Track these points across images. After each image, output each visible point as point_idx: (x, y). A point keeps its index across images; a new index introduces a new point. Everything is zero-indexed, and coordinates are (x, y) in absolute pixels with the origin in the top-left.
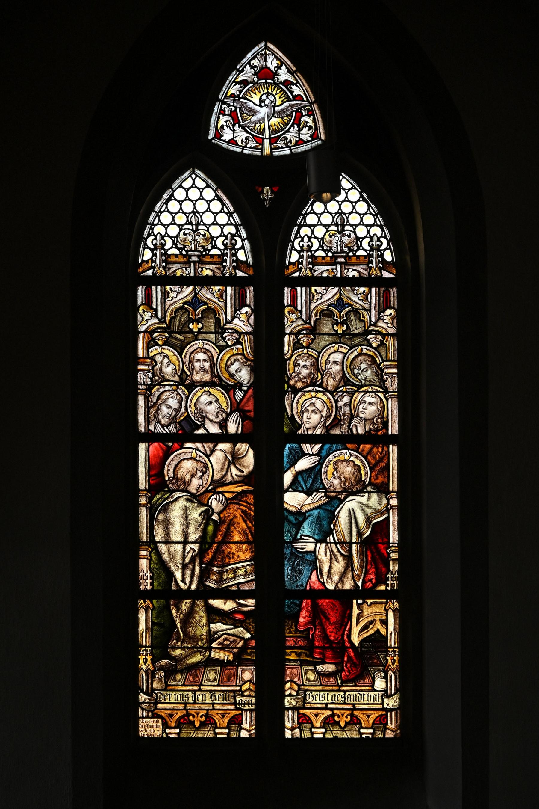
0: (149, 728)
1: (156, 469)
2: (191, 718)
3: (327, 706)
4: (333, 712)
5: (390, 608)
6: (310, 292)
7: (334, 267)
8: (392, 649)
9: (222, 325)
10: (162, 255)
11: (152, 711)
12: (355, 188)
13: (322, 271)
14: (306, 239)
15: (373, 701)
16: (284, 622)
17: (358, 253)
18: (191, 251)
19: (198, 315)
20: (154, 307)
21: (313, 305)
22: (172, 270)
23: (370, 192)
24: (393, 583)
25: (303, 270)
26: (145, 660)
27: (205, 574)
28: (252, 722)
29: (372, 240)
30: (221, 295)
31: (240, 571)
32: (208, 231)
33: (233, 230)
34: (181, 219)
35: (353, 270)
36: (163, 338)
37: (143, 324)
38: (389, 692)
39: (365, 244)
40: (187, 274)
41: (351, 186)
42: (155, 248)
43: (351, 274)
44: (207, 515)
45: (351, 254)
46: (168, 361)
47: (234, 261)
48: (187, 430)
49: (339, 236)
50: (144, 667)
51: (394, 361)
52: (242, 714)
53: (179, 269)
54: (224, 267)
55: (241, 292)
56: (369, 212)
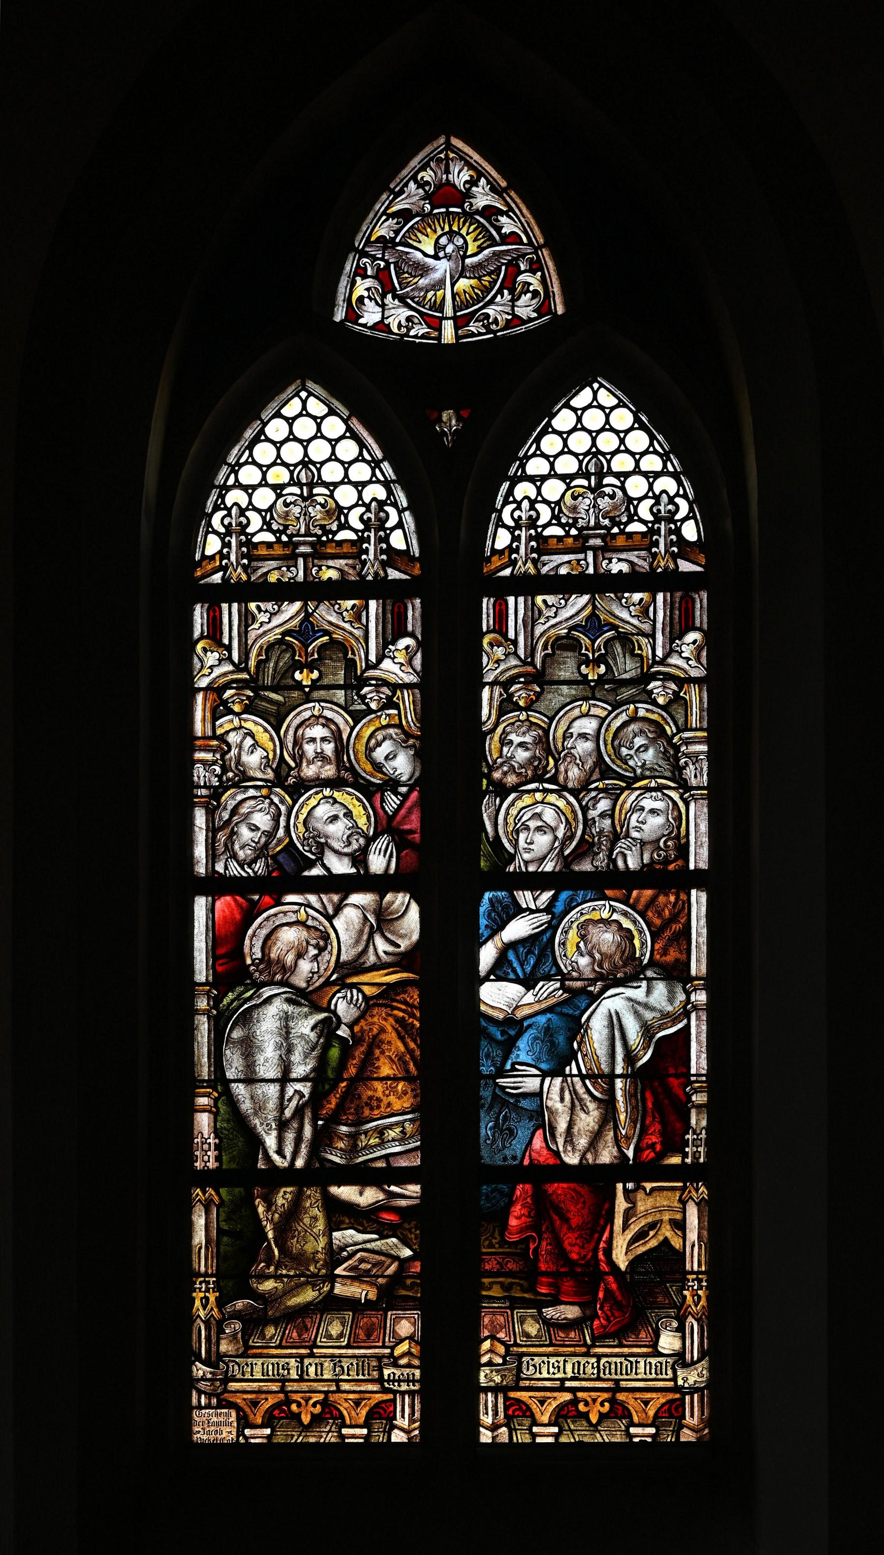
0: (213, 1426)
1: (227, 943)
2: (294, 1407)
4: (575, 1396)
5: (691, 1197)
8: (695, 1276)
9: (359, 672)
10: (240, 544)
11: (218, 1396)
12: (625, 406)
13: (559, 564)
16: (484, 1230)
17: (631, 528)
20: (226, 641)
21: (539, 630)
24: (696, 1150)
25: (520, 563)
26: (204, 1302)
27: (323, 1138)
29: (658, 503)
30: (357, 615)
31: (393, 1132)
33: (381, 493)
38: (688, 1356)
39: (644, 510)
40: (290, 579)
43: (616, 567)
44: (327, 1028)
45: (615, 530)
46: (253, 744)
47: (383, 552)
48: (289, 870)
49: (592, 497)
50: (202, 1313)
51: (701, 729)
52: (394, 1401)
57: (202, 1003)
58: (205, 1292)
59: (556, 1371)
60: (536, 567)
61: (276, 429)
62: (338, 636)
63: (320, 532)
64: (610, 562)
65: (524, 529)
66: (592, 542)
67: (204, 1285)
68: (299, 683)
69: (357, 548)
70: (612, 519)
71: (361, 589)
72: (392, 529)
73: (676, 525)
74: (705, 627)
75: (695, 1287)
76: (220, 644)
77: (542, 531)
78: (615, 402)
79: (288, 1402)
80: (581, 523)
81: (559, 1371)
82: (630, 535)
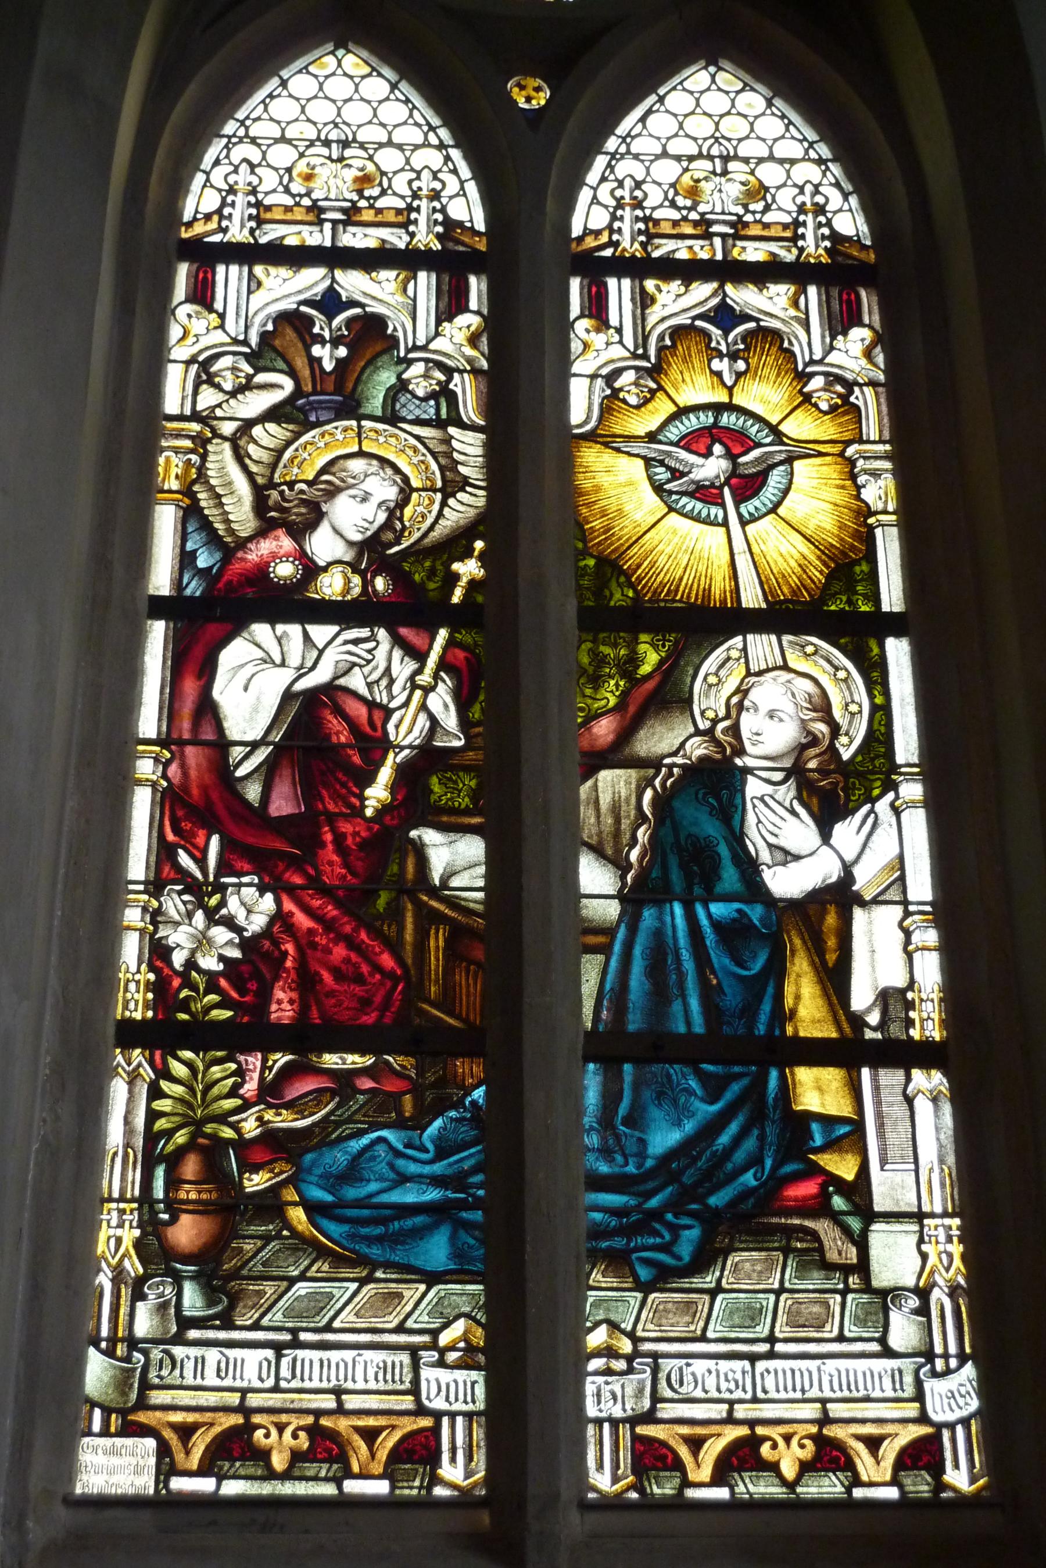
0: (113, 1467)
9: (800, 367)
11: (123, 1412)
28: (618, 1467)
39: (400, 184)
41: (740, 85)
51: (881, 441)
52: (436, 1430)
57: (145, 768)
59: (732, 1386)
60: (645, 249)
66: (715, 229)
71: (408, 261)
74: (485, 312)
79: (250, 1428)
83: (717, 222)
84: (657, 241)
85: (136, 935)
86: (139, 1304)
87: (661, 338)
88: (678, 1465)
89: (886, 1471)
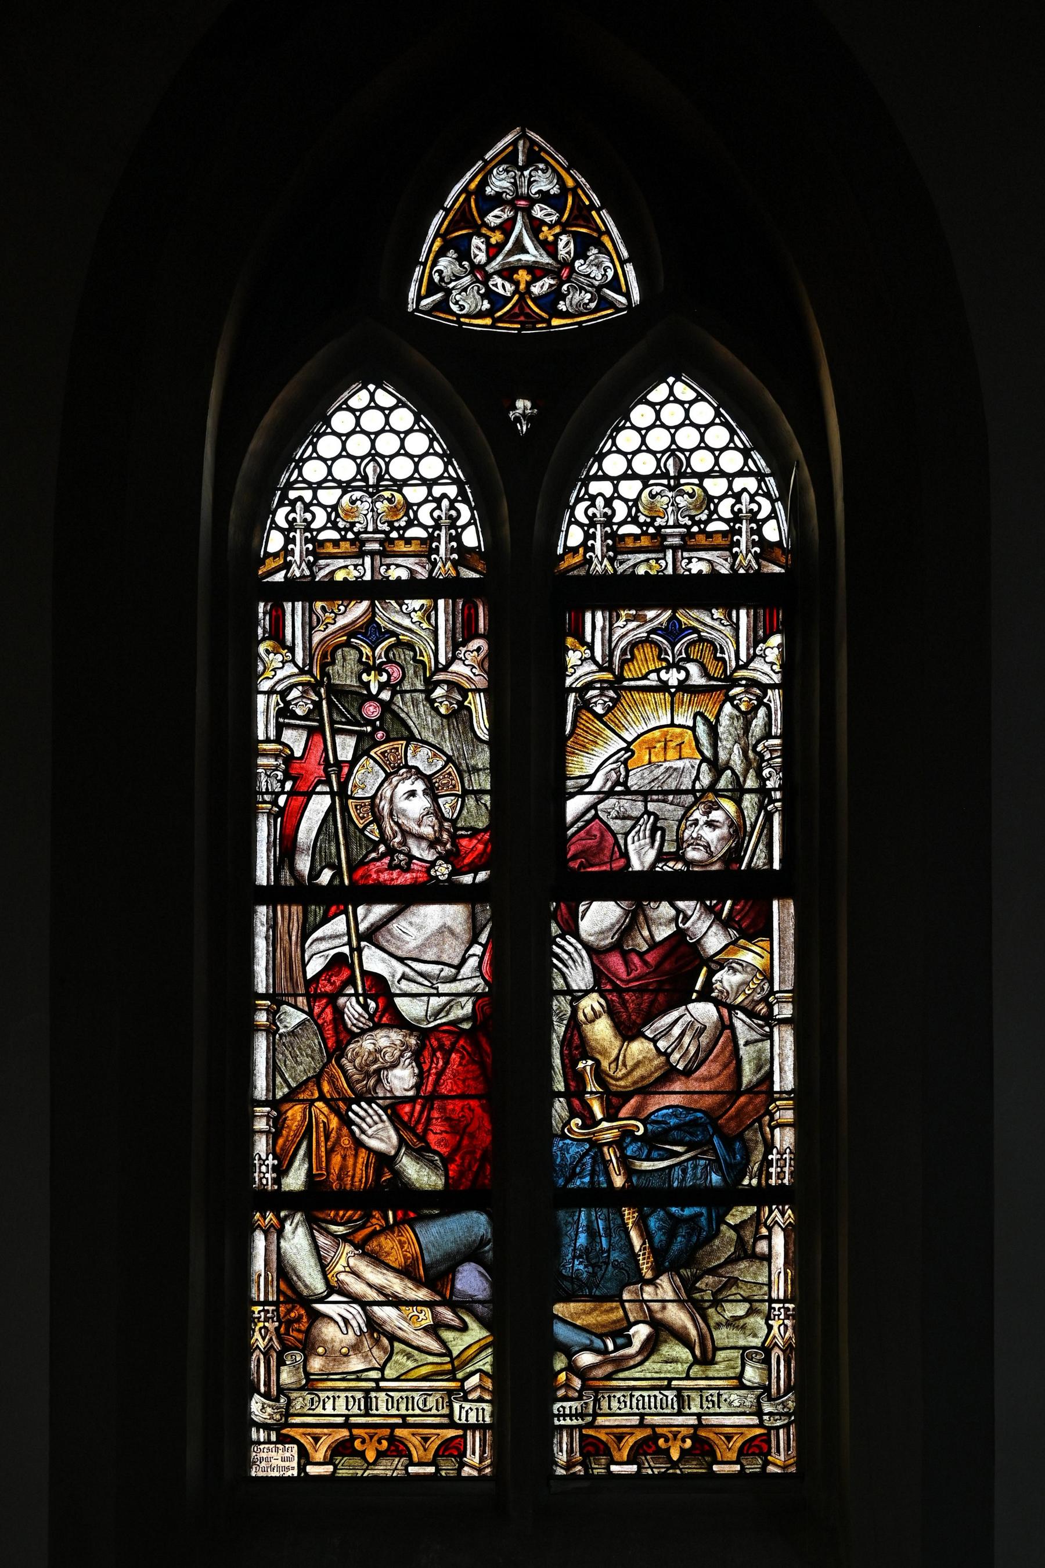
0: (275, 1461)
2: (661, 1441)
3: (642, 1420)
4: (351, 1432)
5: (777, 1222)
6: (312, 611)
7: (360, 561)
8: (261, 1308)
10: (606, 536)
12: (404, 405)
13: (345, 571)
14: (600, 502)
15: (662, 1408)
17: (711, 527)
18: (366, 532)
19: (680, 654)
20: (588, 639)
21: (317, 637)
22: (327, 570)
23: (738, 407)
25: (440, 564)
29: (739, 501)
30: (428, 614)
32: (700, 485)
33: (452, 491)
34: (645, 465)
35: (700, 559)
36: (605, 702)
37: (268, 678)
38: (774, 1390)
40: (357, 578)
42: (592, 524)
43: (394, 574)
45: (695, 529)
47: (754, 544)
49: (370, 500)
50: (262, 1344)
52: (768, 1435)
53: (340, 568)
54: (735, 556)
55: (466, 612)
56: (315, 455)
58: (264, 1322)
61: (342, 421)
62: (406, 637)
63: (387, 529)
64: (690, 562)
65: (598, 526)
67: (262, 1314)
68: (665, 683)
69: (427, 548)
70: (390, 524)
72: (464, 527)
73: (612, 529)
75: (782, 1317)
76: (583, 642)
77: (618, 529)
78: (394, 401)
79: (353, 1438)
80: (659, 522)
81: (713, 1406)
82: (710, 535)
83: (368, 540)
84: (322, 562)
85: (264, 1138)
86: (282, 1368)
87: (624, 652)
88: (607, 1452)
89: (733, 1456)
